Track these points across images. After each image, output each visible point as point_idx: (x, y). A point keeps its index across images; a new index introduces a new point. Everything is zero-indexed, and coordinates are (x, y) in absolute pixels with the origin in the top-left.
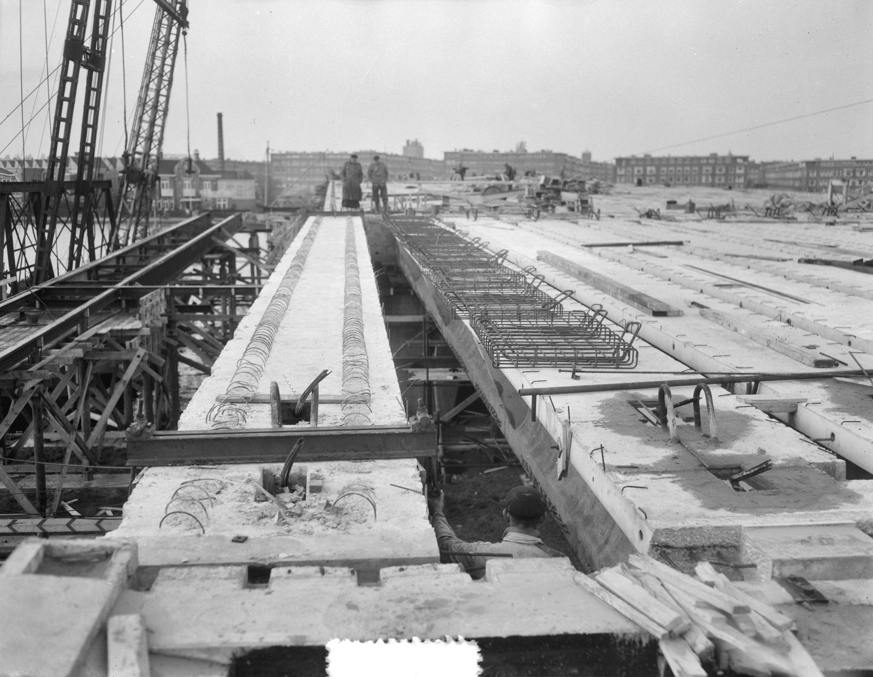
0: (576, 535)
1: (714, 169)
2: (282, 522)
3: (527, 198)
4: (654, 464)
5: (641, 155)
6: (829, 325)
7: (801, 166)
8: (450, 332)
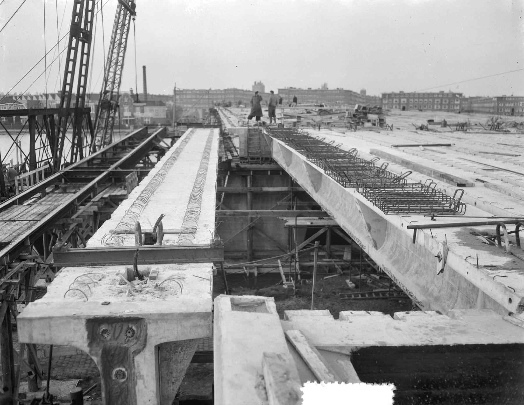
1: (442, 101)
3: (347, 117)
4: (503, 265)
5: (397, 91)
7: (494, 99)
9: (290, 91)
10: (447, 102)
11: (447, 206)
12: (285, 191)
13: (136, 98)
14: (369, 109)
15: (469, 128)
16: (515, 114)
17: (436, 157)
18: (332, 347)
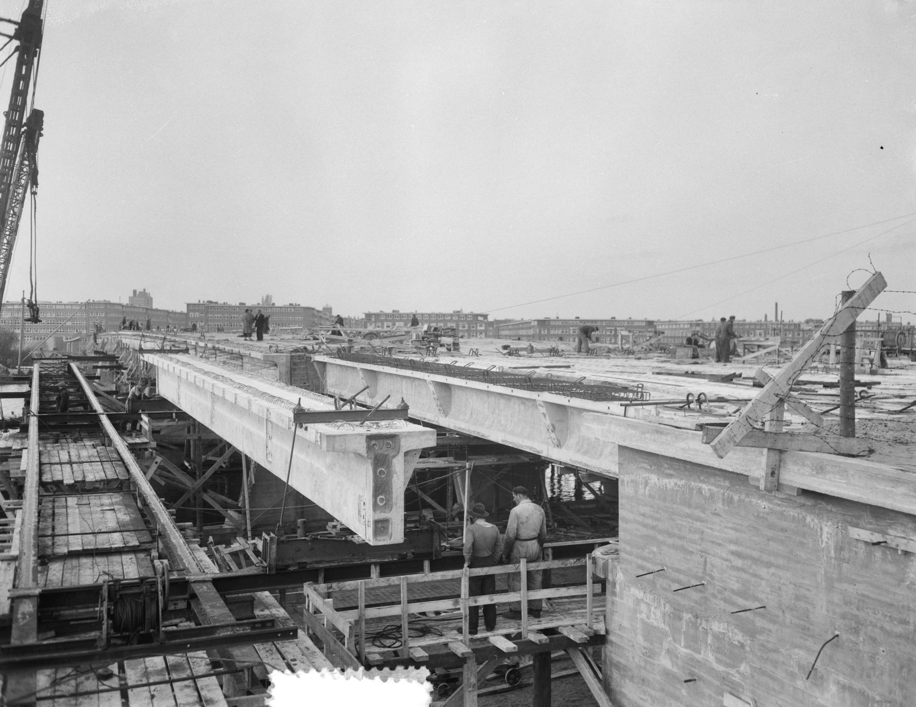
5: (388, 310)
7: (532, 324)
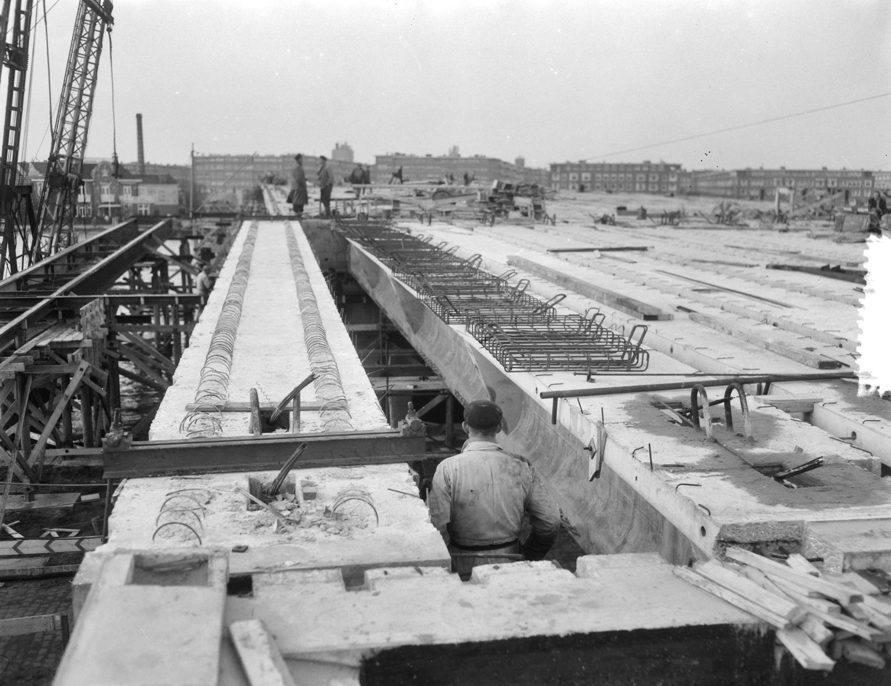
0: (589, 537)
1: (647, 177)
2: (281, 530)
3: (480, 202)
4: (698, 462)
5: (575, 160)
6: (818, 329)
8: (419, 340)
9: (397, 158)
10: (657, 179)
11: (617, 356)
12: (372, 331)
13: (118, 171)
14: (515, 187)
15: (682, 220)
16: (765, 197)
17: (619, 269)
18: (320, 653)
